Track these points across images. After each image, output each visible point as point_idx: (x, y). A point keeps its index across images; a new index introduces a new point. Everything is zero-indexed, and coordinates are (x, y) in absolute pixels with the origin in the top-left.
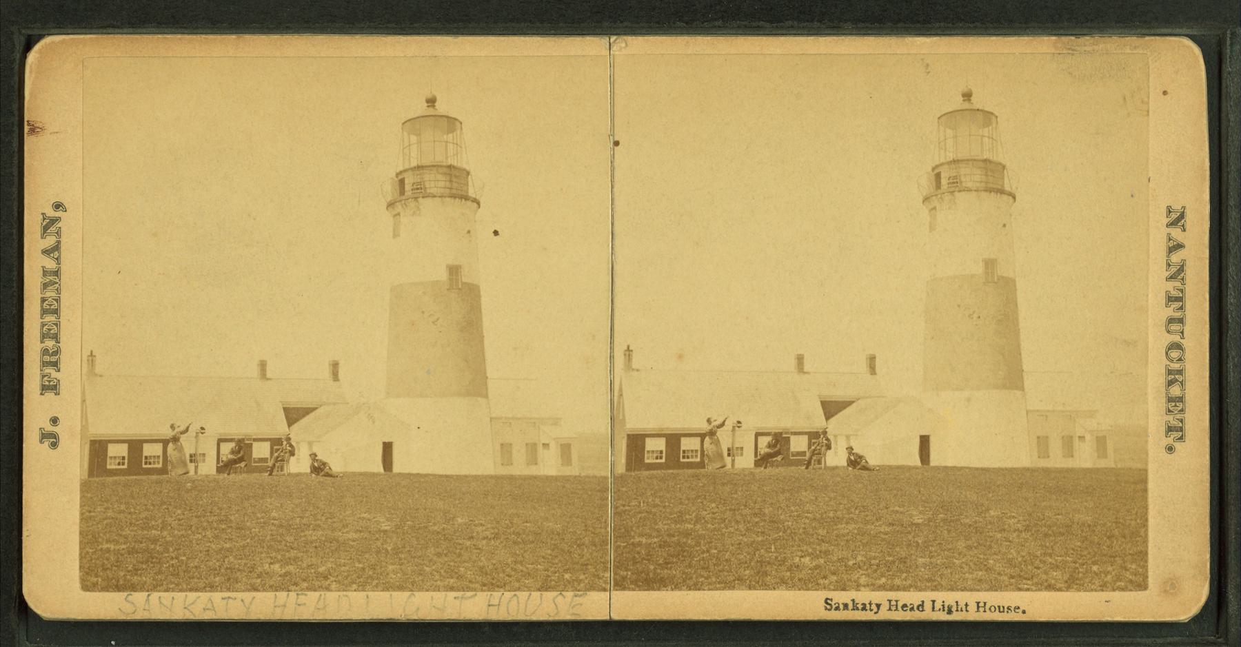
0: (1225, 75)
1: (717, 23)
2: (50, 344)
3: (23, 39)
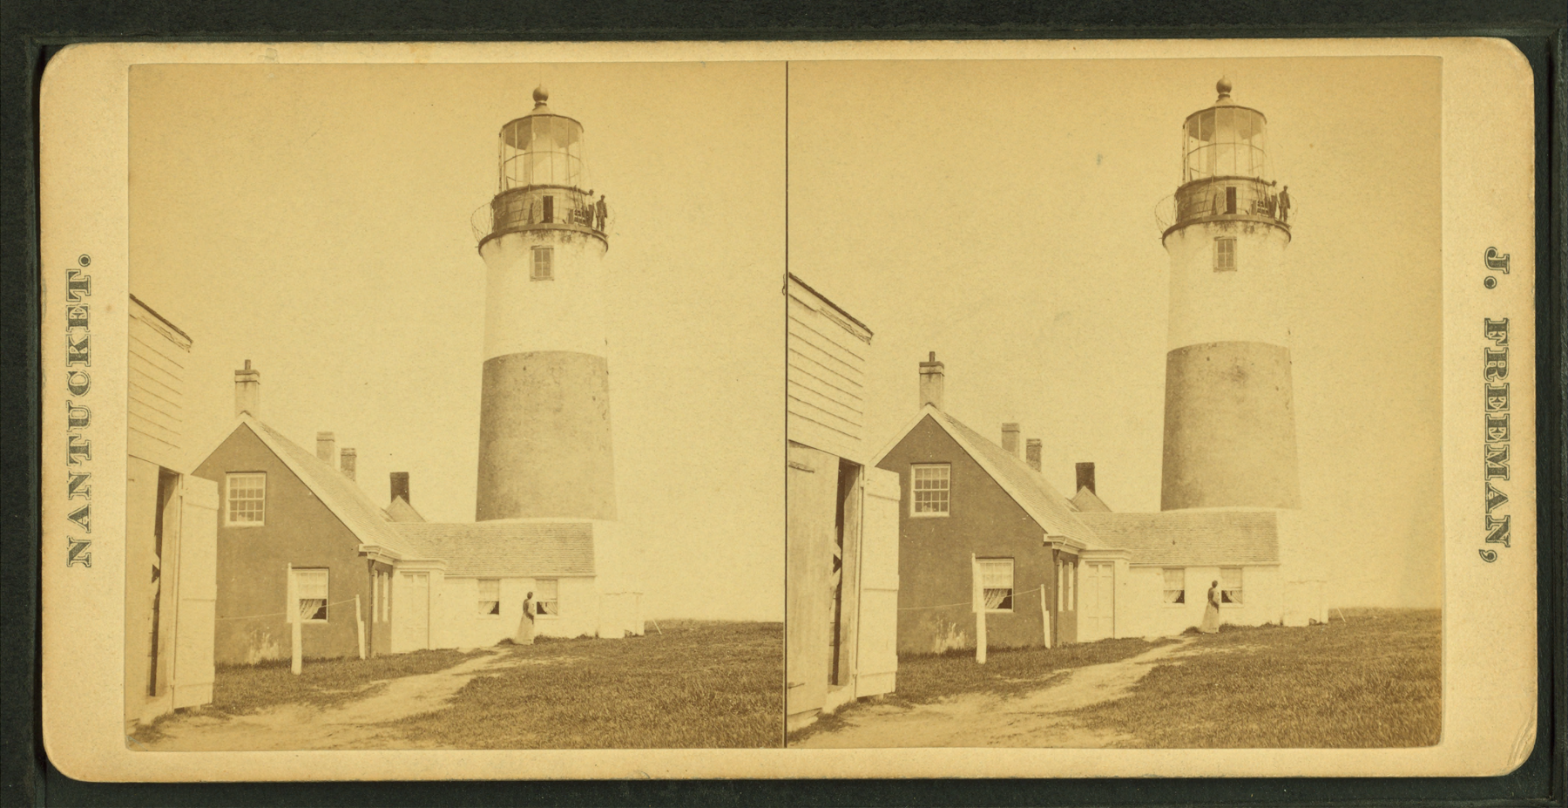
0: (1557, 87)
1: (914, 26)
2: (1498, 383)
3: (36, 50)
